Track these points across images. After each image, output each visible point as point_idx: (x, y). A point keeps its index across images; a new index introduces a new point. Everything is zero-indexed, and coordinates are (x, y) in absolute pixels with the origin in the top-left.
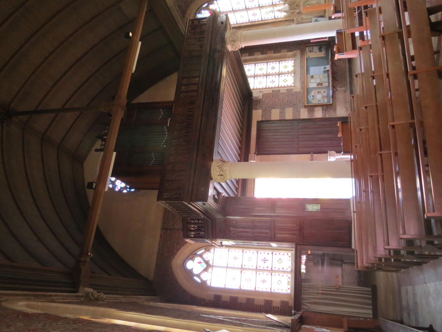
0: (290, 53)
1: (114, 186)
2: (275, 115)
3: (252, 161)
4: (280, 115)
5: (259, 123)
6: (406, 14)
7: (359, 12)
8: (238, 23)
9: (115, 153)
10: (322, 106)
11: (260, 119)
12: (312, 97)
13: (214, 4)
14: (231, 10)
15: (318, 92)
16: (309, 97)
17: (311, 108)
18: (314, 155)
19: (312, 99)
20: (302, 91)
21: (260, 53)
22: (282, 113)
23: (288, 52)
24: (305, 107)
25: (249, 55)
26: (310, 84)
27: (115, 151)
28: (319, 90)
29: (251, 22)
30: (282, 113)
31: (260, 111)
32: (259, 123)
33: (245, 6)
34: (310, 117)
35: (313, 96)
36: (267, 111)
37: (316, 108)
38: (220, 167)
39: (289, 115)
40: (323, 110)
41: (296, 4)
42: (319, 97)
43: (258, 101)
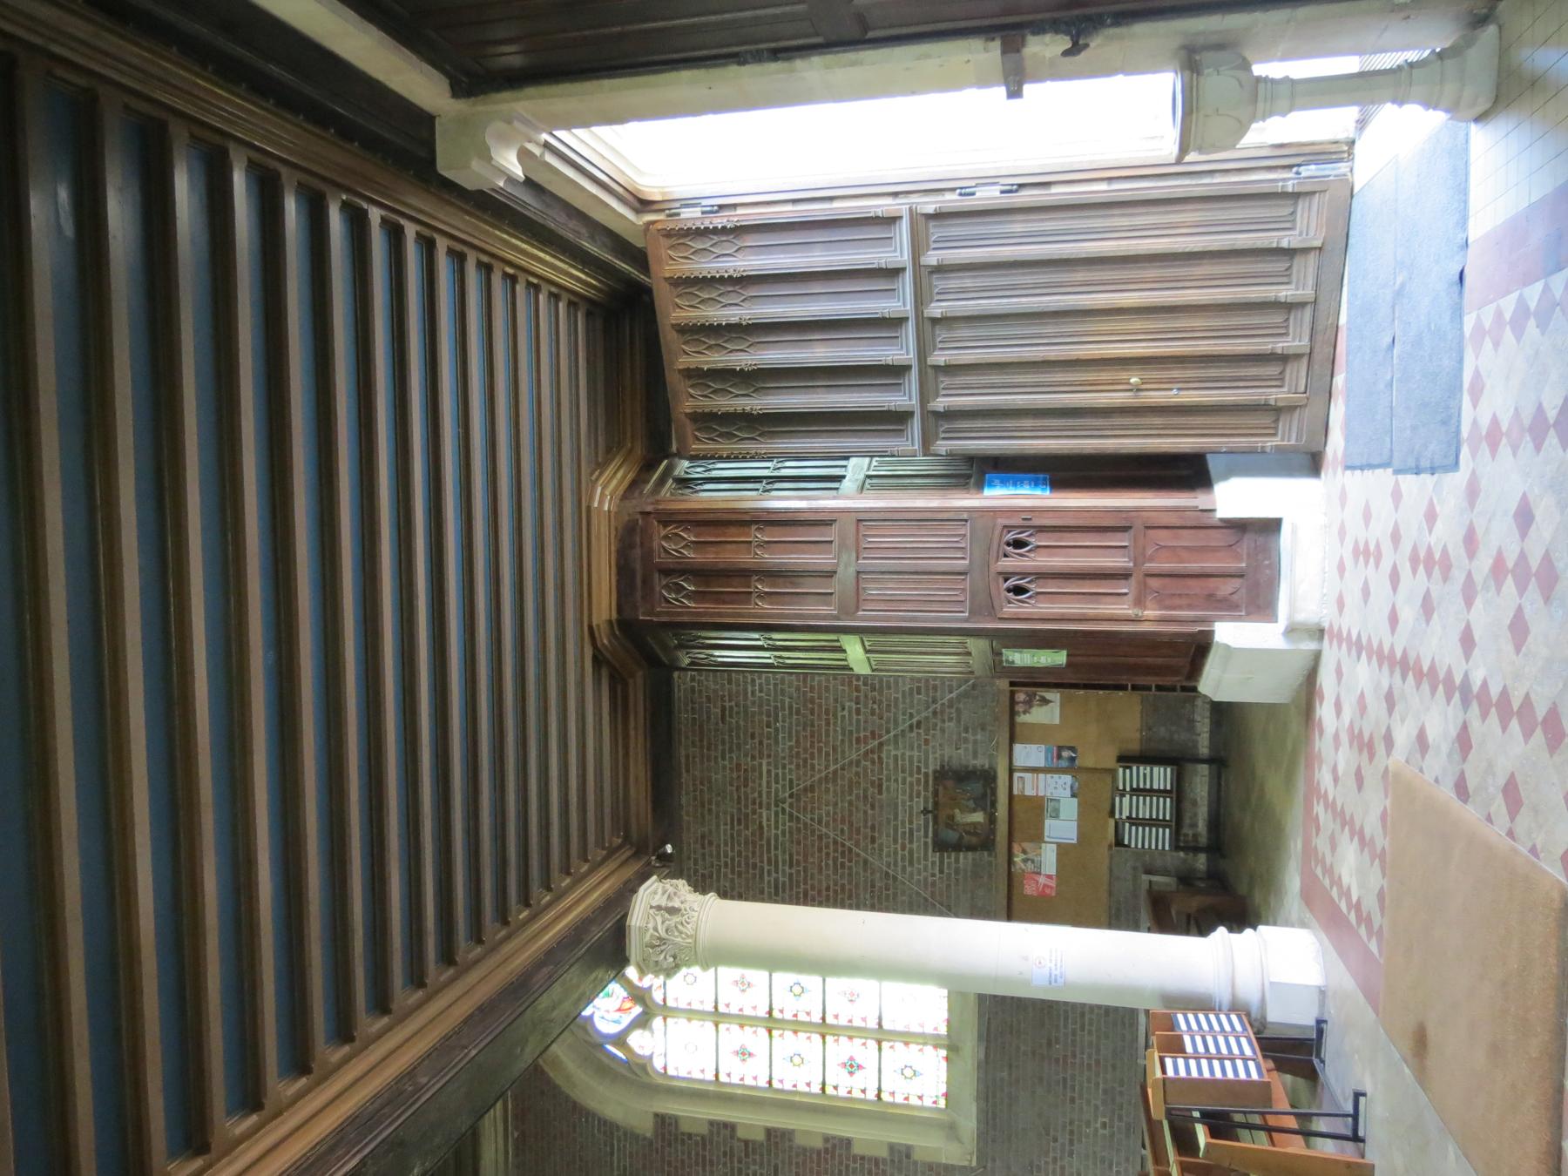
13: (652, 1031)
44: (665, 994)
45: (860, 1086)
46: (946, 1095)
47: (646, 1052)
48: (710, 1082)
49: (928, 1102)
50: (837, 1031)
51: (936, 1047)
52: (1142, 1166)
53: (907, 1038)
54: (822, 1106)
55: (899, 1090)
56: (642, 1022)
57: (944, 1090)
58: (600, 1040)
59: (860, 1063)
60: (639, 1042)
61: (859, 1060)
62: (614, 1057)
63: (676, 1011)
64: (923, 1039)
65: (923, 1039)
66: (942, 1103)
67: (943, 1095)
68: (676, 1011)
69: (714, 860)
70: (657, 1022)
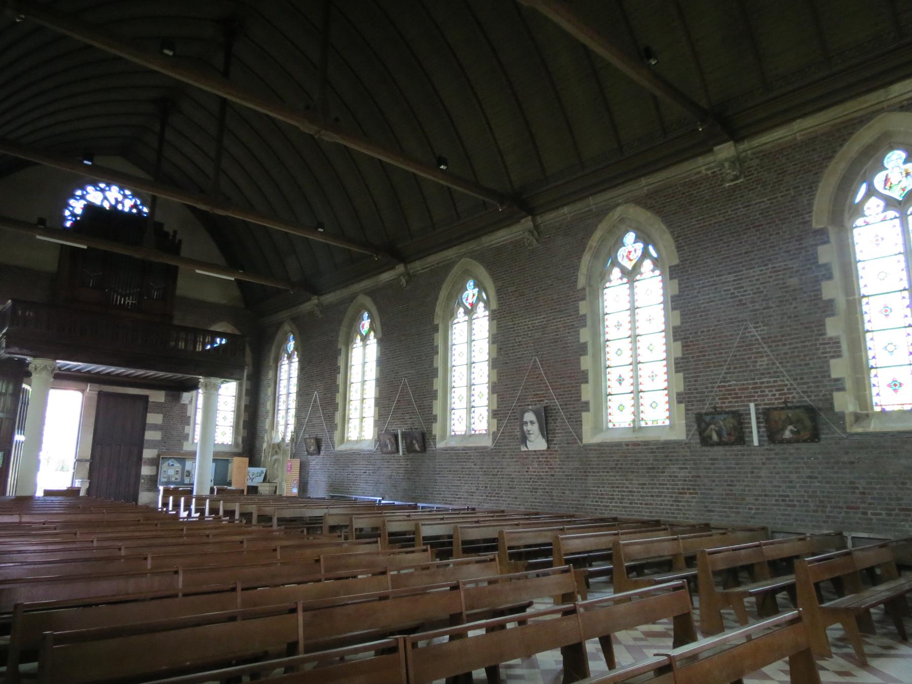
0: (240, 440)
1: (78, 198)
2: (153, 418)
3: (88, 388)
4: (153, 424)
5: (146, 398)
6: (482, 632)
7: (837, 597)
8: (281, 381)
9: (85, 247)
10: (157, 475)
11: (151, 400)
12: (171, 464)
13: (485, 311)
14: (637, 304)
15: (177, 471)
16: (173, 460)
17: (155, 463)
18: (89, 463)
19: (169, 464)
20: (183, 452)
21: (248, 403)
22: (155, 427)
23: (243, 438)
24: (159, 456)
25: (247, 390)
26: (191, 462)
27: (88, 247)
28: (180, 473)
29: (278, 397)
30: (155, 427)
31: (162, 400)
32: (146, 398)
33: (866, 294)
34: (143, 460)
35: (173, 465)
36: (159, 408)
37: (155, 468)
38: (45, 368)
39: (150, 435)
40: (151, 476)
41: (278, 450)
42: (171, 472)
43: (178, 398)
44: (860, 226)
45: (612, 385)
46: (883, 411)
47: (867, 212)
48: (603, 311)
49: (875, 399)
50: (635, 371)
51: (634, 421)
52: (714, 528)
53: (637, 405)
54: (600, 368)
55: (613, 403)
56: (625, 272)
57: (888, 409)
58: (613, 255)
59: (655, 379)
60: (616, 273)
61: (623, 383)
62: (856, 193)
63: (632, 288)
64: (637, 413)
65: (637, 413)
66: (877, 409)
67: (884, 409)
68: (632, 288)
69: (774, 278)
70: (892, 213)
